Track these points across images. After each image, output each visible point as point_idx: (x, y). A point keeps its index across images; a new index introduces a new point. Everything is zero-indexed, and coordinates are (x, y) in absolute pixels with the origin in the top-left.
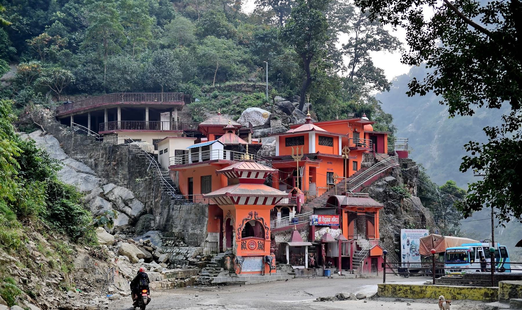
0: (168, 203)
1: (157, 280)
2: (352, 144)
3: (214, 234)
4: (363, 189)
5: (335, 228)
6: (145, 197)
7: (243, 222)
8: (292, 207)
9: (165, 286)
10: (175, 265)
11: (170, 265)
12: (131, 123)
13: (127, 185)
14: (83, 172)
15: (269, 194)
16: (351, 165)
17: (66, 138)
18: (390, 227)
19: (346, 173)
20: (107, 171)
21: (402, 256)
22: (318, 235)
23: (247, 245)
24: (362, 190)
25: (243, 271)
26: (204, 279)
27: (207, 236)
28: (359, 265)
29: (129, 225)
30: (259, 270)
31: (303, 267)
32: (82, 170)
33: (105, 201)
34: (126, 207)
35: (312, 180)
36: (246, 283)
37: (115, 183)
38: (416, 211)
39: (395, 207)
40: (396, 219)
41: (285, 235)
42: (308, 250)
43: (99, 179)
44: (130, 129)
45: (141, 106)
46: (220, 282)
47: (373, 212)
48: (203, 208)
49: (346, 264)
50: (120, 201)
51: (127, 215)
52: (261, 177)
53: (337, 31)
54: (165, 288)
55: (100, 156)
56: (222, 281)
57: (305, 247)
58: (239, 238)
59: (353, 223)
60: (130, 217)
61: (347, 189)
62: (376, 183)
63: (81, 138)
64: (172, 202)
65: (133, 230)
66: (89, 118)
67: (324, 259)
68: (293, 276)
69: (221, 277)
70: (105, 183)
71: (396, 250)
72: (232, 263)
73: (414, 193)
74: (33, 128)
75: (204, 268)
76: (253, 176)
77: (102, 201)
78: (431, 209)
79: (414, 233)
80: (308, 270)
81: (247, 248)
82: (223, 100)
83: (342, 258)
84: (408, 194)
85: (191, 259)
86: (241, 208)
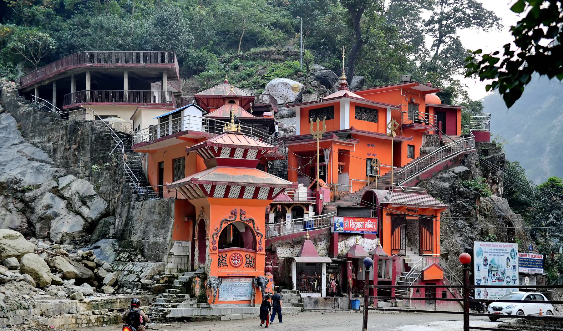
0: (129, 199)
1: (69, 313)
2: (406, 120)
3: (184, 243)
4: (418, 182)
5: (370, 237)
6: (108, 192)
7: (221, 225)
8: (307, 206)
10: (125, 289)
11: (118, 289)
13: (89, 177)
14: (37, 160)
15: (262, 182)
16: (405, 151)
17: (24, 116)
18: (458, 239)
19: (397, 162)
20: (67, 159)
22: (342, 247)
23: (227, 260)
26: (156, 311)
27: (172, 245)
29: (83, 231)
31: (318, 295)
32: (36, 158)
33: (57, 199)
34: (84, 207)
35: (343, 169)
36: (222, 318)
37: (75, 175)
38: (499, 217)
39: (467, 210)
40: (468, 228)
41: (293, 247)
42: (327, 269)
43: (57, 169)
44: (101, 101)
45: (118, 70)
48: (168, 204)
49: (387, 291)
50: (77, 198)
51: (83, 217)
52: (251, 156)
53: (419, 8)
54: (84, 326)
55: (60, 138)
57: (321, 264)
58: (214, 249)
59: (398, 230)
60: (86, 221)
61: (394, 182)
62: (440, 175)
63: (41, 115)
64: (134, 197)
65: (88, 239)
66: (54, 89)
67: (355, 284)
68: (300, 308)
70: (62, 174)
72: (203, 287)
73: (498, 192)
75: (160, 295)
76: (238, 155)
77: (53, 198)
78: (526, 218)
79: (495, 248)
80: (326, 299)
81: (228, 264)
82: (244, 71)
84: (486, 191)
85: (144, 281)
86: (218, 202)
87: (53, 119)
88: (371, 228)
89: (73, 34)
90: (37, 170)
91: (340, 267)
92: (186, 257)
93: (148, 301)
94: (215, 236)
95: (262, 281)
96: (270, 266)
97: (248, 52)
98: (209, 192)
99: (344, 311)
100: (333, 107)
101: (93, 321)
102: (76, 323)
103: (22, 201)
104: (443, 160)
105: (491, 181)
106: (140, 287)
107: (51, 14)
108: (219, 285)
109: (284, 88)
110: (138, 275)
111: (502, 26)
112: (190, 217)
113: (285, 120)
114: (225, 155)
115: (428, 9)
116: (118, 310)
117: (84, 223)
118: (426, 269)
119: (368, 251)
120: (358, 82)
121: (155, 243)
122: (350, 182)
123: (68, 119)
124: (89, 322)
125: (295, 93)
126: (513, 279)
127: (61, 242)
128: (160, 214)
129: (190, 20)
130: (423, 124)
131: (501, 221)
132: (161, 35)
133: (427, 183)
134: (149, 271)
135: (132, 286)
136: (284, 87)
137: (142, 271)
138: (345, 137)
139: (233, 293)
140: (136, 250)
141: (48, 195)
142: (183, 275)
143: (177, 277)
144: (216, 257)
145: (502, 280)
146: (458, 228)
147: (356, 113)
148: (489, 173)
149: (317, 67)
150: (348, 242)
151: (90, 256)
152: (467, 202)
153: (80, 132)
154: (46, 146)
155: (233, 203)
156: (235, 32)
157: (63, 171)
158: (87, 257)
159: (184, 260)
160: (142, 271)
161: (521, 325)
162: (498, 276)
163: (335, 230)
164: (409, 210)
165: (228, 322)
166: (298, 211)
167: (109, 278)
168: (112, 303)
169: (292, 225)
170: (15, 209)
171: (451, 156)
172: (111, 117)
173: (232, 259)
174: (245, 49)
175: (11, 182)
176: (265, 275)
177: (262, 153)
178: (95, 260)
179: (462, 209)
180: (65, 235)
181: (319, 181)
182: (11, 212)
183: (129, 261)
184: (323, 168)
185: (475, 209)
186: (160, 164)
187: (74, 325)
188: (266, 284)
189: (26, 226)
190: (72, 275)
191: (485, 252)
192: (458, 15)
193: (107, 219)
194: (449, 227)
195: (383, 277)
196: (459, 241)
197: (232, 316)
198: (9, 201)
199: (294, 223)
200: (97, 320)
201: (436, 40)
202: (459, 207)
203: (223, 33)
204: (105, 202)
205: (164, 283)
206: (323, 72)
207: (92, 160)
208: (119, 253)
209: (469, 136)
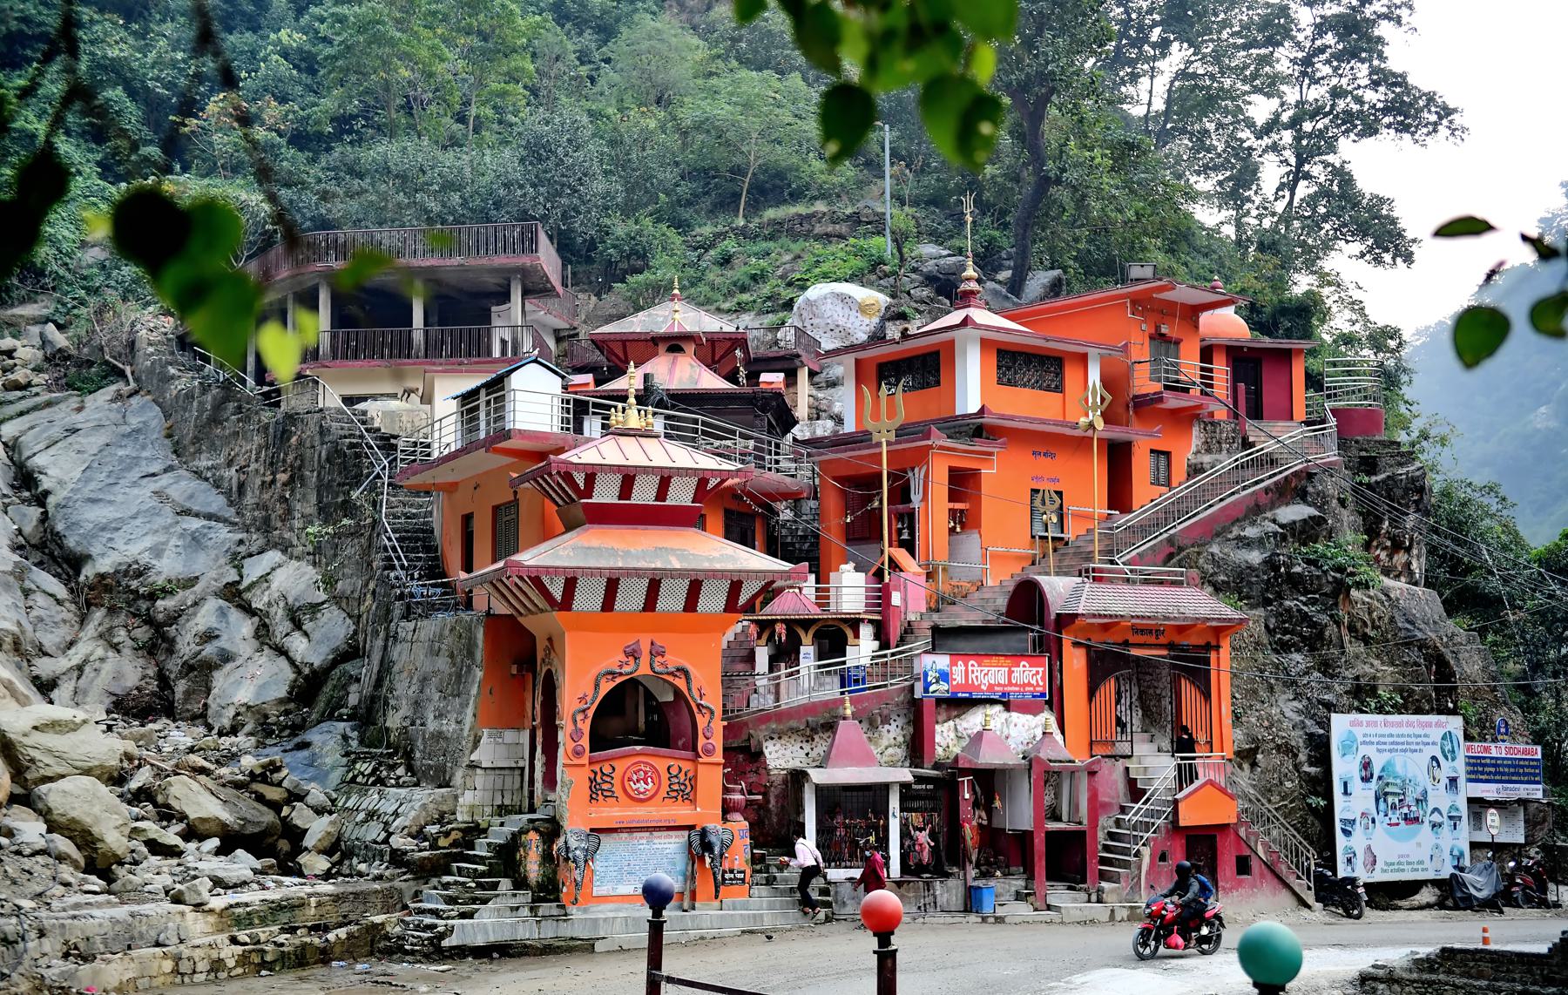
0: (386, 615)
1: (158, 944)
2: (1144, 383)
3: (509, 736)
4: (1173, 553)
5: (1028, 708)
6: (356, 595)
7: (597, 686)
9: (202, 966)
10: (355, 861)
11: (340, 863)
12: (361, 338)
14: (197, 515)
15: (706, 565)
16: (1142, 466)
18: (1287, 708)
19: (1119, 497)
21: (1338, 826)
22: (946, 738)
23: (616, 782)
24: (1171, 556)
26: (418, 928)
27: (476, 743)
28: (1126, 865)
32: (196, 508)
33: (235, 615)
34: (297, 634)
35: (964, 521)
36: (599, 946)
37: (284, 551)
39: (1313, 625)
40: (1316, 674)
43: (243, 536)
46: (480, 941)
50: (280, 612)
51: (292, 662)
52: (681, 495)
57: (885, 787)
58: (578, 753)
60: (298, 671)
62: (1236, 531)
65: (298, 720)
67: (979, 838)
69: (494, 920)
70: (254, 549)
72: (547, 858)
73: (1411, 573)
74: (105, 377)
75: (434, 881)
76: (643, 494)
79: (1395, 731)
81: (618, 791)
82: (745, 269)
83: (1050, 835)
84: (1367, 572)
85: (398, 842)
86: (585, 623)
87: (240, 407)
88: (1029, 684)
89: (326, 192)
92: (517, 772)
94: (580, 717)
95: (713, 839)
96: (737, 797)
97: (757, 220)
99: (949, 920)
100: (937, 353)
101: (231, 963)
102: (176, 971)
103: (149, 621)
104: (1244, 488)
105: (1389, 543)
106: (387, 858)
107: (273, 146)
108: (590, 854)
109: (839, 309)
110: (386, 823)
111: (1464, 130)
112: (518, 660)
114: (605, 493)
115: (1269, 96)
116: (311, 929)
117: (292, 676)
118: (1186, 797)
119: (1021, 748)
120: (1044, 286)
121: (439, 736)
123: (277, 404)
124: (217, 966)
125: (867, 321)
126: (1451, 818)
127: (234, 731)
128: (452, 656)
129: (613, 143)
130: (1195, 391)
131: (1414, 655)
132: (534, 186)
133: (1199, 553)
134: (413, 813)
136: (841, 308)
137: (396, 814)
140: (395, 753)
141: (213, 604)
143: (485, 831)
144: (586, 773)
147: (999, 367)
148: (1381, 521)
149: (929, 249)
150: (965, 724)
152: (1313, 604)
153: (294, 440)
154: (222, 477)
155: (629, 623)
156: (732, 171)
157: (257, 540)
158: (263, 775)
159: (512, 781)
160: (396, 814)
161: (1425, 976)
162: (1405, 810)
163: (926, 690)
164: (1137, 630)
165: (613, 958)
166: (834, 637)
167: (317, 829)
168: (293, 907)
169: (817, 677)
170: (130, 643)
171: (1268, 479)
172: (374, 397)
174: (755, 207)
175: (126, 574)
176: (725, 819)
177: (710, 486)
178: (285, 784)
179: (1300, 624)
180: (243, 710)
182: (119, 651)
183: (374, 784)
185: (1338, 623)
186: (467, 519)
187: (169, 979)
188: (725, 846)
189: (154, 686)
190: (214, 827)
191: (1364, 743)
192: (1341, 104)
193: (348, 666)
195: (1065, 817)
196: (1289, 714)
198: (116, 622)
200: (243, 960)
201: (1288, 174)
202: (1291, 617)
203: (702, 174)
204: (348, 621)
205: (452, 845)
206: (942, 262)
207: (320, 510)
208: (354, 762)
209: (1323, 421)
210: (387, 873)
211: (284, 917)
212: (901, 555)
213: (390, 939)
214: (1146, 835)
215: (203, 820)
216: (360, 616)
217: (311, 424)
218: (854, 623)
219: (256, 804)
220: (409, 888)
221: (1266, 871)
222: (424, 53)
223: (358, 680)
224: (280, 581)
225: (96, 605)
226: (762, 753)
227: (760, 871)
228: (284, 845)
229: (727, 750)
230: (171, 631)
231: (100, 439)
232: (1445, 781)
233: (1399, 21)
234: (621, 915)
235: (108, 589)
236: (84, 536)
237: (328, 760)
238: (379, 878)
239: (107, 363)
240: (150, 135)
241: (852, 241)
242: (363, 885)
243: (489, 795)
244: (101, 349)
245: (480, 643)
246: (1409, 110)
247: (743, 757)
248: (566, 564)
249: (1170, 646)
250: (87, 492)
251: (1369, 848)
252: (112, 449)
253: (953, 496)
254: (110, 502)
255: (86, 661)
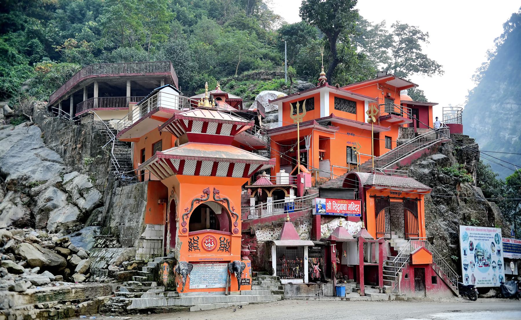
0: (112, 187)
2: (383, 112)
3: (157, 227)
5: (354, 220)
7: (192, 205)
10: (95, 276)
14: (49, 161)
15: (236, 157)
19: (376, 152)
21: (463, 266)
22: (325, 230)
25: (192, 286)
27: (144, 229)
28: (393, 279)
29: (77, 221)
30: (221, 285)
31: (299, 281)
32: (49, 159)
33: (60, 193)
34: (81, 198)
35: (324, 156)
36: (192, 309)
37: (79, 172)
40: (450, 212)
41: (273, 230)
42: (309, 252)
43: (65, 167)
46: (143, 307)
47: (414, 198)
49: (372, 276)
50: (76, 191)
51: (79, 208)
56: (148, 306)
57: (303, 247)
58: (184, 231)
59: (383, 213)
60: (81, 211)
62: (419, 162)
64: (116, 183)
67: (336, 268)
68: (280, 296)
71: (453, 257)
72: (172, 273)
74: (23, 120)
75: (125, 283)
76: (211, 131)
79: (480, 232)
80: (308, 285)
82: (238, 89)
83: (365, 267)
85: (111, 268)
86: (188, 180)
87: (66, 125)
90: (47, 168)
91: (324, 251)
92: (160, 241)
93: (111, 290)
94: (185, 217)
95: (238, 266)
96: (247, 250)
98: (177, 168)
99: (329, 299)
100: (313, 98)
103: (29, 195)
104: (421, 148)
110: (107, 261)
111: (443, 72)
112: (162, 198)
113: (272, 124)
114: (197, 130)
115: (384, 63)
116: (72, 302)
117: (79, 213)
118: (415, 253)
119: (353, 234)
121: (130, 228)
122: (331, 169)
126: (499, 265)
128: (135, 198)
134: (118, 257)
135: (101, 273)
137: (111, 257)
138: (324, 125)
139: (205, 281)
140: (113, 236)
141: (52, 189)
142: (153, 261)
143: (146, 263)
144: (187, 240)
145: (488, 265)
146: (441, 213)
147: (335, 103)
151: (64, 243)
152: (447, 188)
153: (83, 133)
154: (59, 149)
157: (70, 168)
158: (61, 244)
159: (158, 245)
160: (111, 257)
162: (484, 261)
163: (317, 211)
165: (198, 313)
166: (279, 193)
167: (81, 264)
168: (64, 293)
170: (21, 202)
173: (205, 242)
174: (239, 74)
175: (21, 179)
176: (242, 259)
178: (69, 247)
180: (60, 224)
181: (300, 166)
182: (17, 206)
183: (104, 247)
184: (304, 154)
185: (456, 195)
186: (143, 151)
188: (243, 269)
189: (28, 217)
190: (38, 263)
191: (470, 236)
194: (431, 212)
195: (369, 261)
196: (442, 226)
197: (201, 305)
198: (17, 195)
199: (275, 206)
204: (100, 194)
208: (97, 240)
210: (106, 280)
211: (60, 297)
212: (303, 167)
213: (105, 306)
214: (400, 268)
215: (33, 260)
216: (104, 191)
217: (89, 127)
218: (288, 188)
219: (57, 255)
220: (115, 286)
221: (442, 282)
222: (134, 23)
223: (101, 212)
224: (76, 181)
225: (10, 190)
226: (255, 234)
227: (255, 280)
228: (68, 271)
229: (243, 233)
230: (36, 198)
231: (19, 138)
232: (496, 251)
233: (424, 40)
234: (201, 296)
235: (15, 184)
236: (8, 167)
237: (88, 240)
238: (103, 282)
239: (24, 115)
240: (47, 54)
241: (273, 80)
242: (95, 285)
243: (148, 250)
244: (22, 111)
245: (146, 191)
246: (427, 66)
247: (248, 235)
248: (181, 154)
249: (403, 199)
250: (11, 154)
251: (473, 275)
252: (22, 141)
253: (320, 148)
254: (19, 157)
255: (4, 209)
